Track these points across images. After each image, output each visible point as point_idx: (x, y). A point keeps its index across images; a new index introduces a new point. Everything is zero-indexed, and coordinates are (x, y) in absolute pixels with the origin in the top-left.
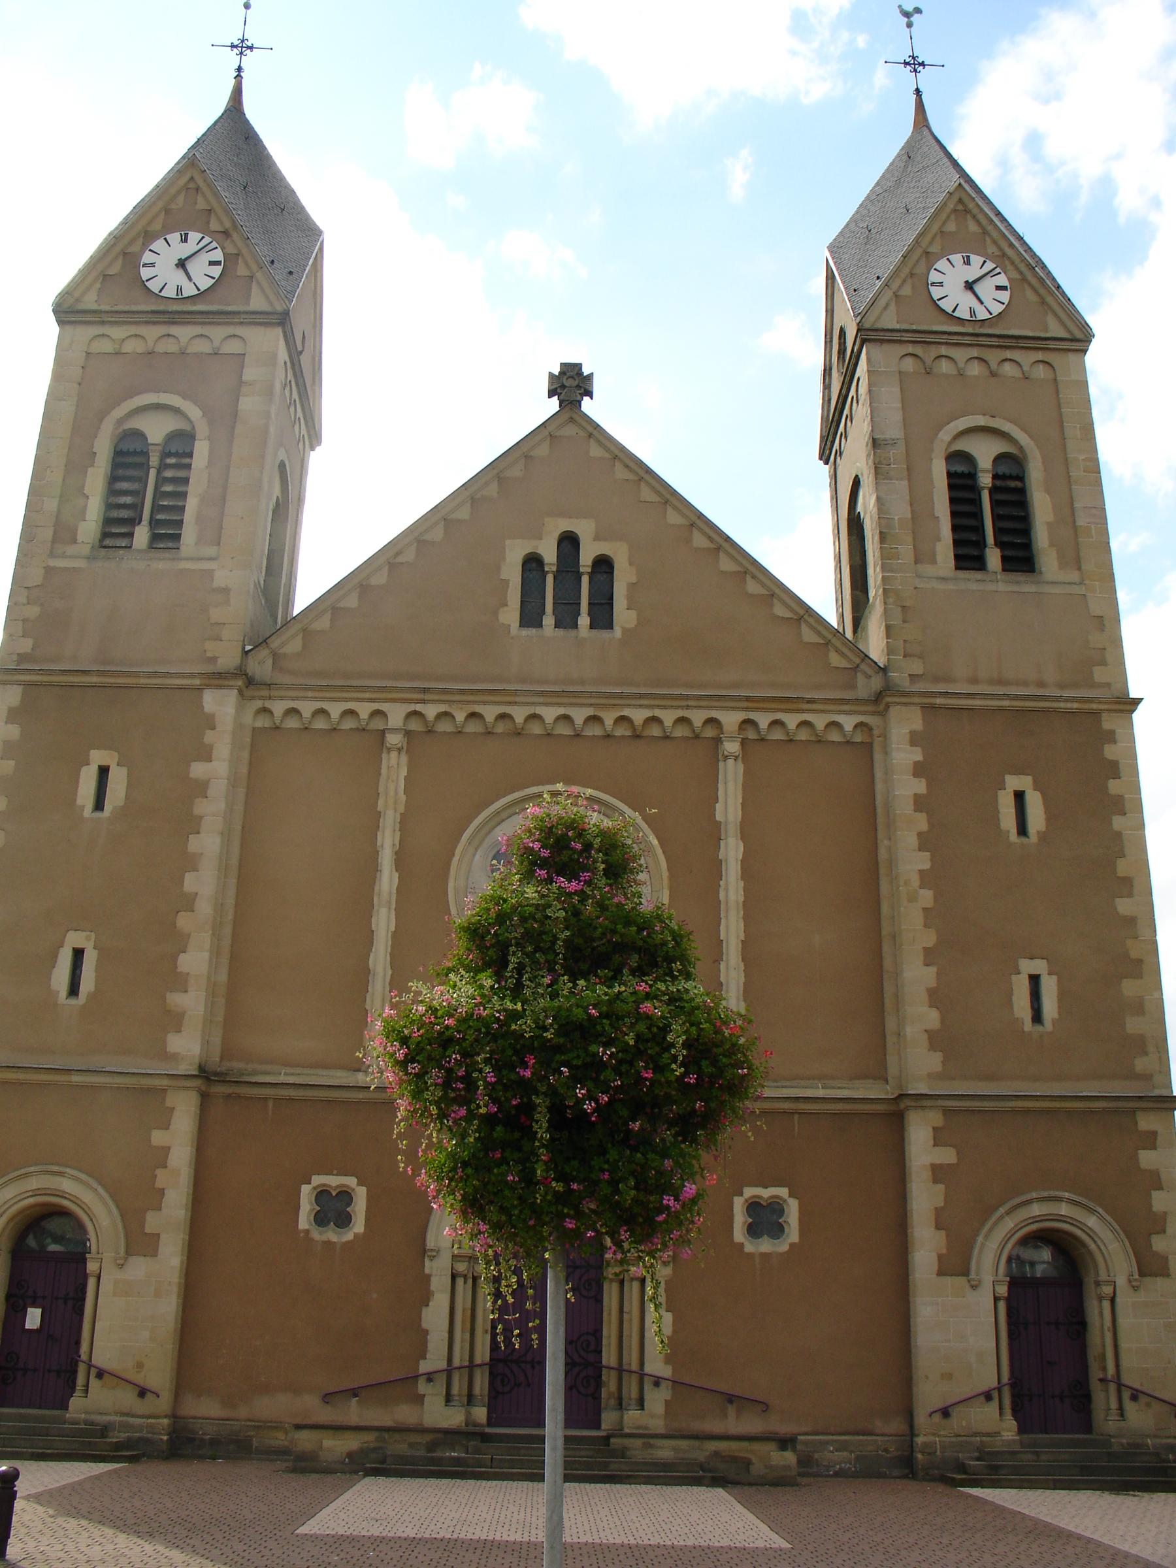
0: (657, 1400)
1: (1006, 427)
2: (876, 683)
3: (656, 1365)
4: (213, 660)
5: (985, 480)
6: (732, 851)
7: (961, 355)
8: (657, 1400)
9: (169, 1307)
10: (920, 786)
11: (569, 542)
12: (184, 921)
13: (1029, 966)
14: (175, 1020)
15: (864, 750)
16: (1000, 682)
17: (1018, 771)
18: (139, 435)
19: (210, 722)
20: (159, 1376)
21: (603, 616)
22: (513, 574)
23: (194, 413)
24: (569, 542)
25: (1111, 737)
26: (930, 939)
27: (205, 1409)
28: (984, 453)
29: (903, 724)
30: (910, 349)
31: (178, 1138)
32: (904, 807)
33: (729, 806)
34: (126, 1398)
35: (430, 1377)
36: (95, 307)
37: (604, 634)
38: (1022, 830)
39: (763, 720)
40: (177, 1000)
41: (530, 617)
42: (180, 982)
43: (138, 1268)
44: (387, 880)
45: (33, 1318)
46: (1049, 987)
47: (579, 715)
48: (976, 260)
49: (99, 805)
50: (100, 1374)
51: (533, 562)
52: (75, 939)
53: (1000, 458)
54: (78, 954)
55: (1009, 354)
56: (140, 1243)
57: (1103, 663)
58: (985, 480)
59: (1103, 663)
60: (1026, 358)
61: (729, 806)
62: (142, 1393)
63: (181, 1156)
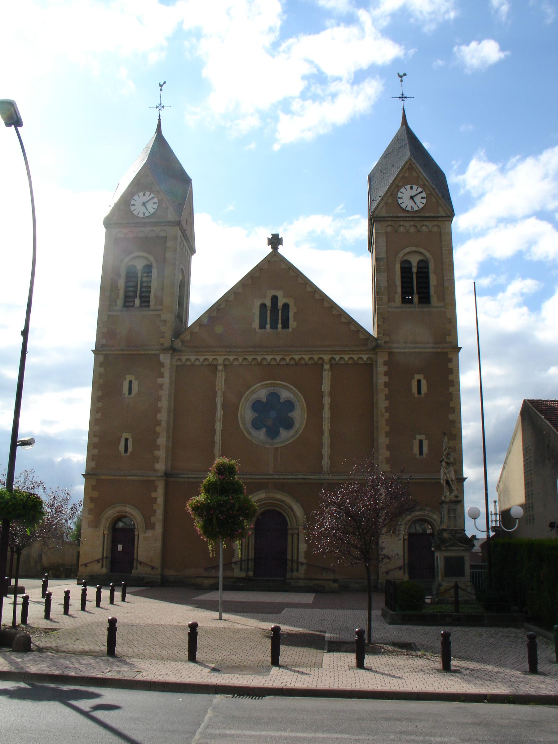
0: (302, 569)
1: (422, 251)
2: (374, 344)
3: (302, 559)
4: (162, 344)
5: (414, 270)
6: (327, 401)
7: (407, 224)
8: (302, 569)
9: (159, 544)
10: (386, 379)
11: (275, 299)
12: (158, 429)
13: (419, 437)
14: (157, 459)
15: (370, 366)
16: (415, 342)
17: (419, 373)
18: (408, 262)
19: (162, 365)
20: (157, 563)
21: (286, 325)
22: (256, 311)
23: (152, 259)
24: (275, 299)
25: (451, 360)
26: (387, 429)
27: (171, 573)
28: (414, 260)
29: (381, 358)
30: (390, 223)
31: (159, 495)
32: (381, 386)
33: (326, 386)
34: (149, 570)
35: (236, 563)
36: (386, 215)
37: (286, 330)
38: (419, 392)
39: (337, 357)
40: (157, 453)
41: (262, 326)
42: (158, 448)
43: (150, 533)
44: (219, 413)
45: (120, 547)
46: (425, 444)
47: (278, 358)
48: (415, 187)
49: (130, 393)
50: (141, 563)
51: (263, 306)
52: (125, 435)
53: (420, 262)
54: (127, 440)
55: (424, 223)
56: (149, 526)
57: (450, 335)
58: (414, 270)
59: (450, 335)
60: (430, 224)
61: (326, 386)
62: (153, 568)
63: (160, 500)
